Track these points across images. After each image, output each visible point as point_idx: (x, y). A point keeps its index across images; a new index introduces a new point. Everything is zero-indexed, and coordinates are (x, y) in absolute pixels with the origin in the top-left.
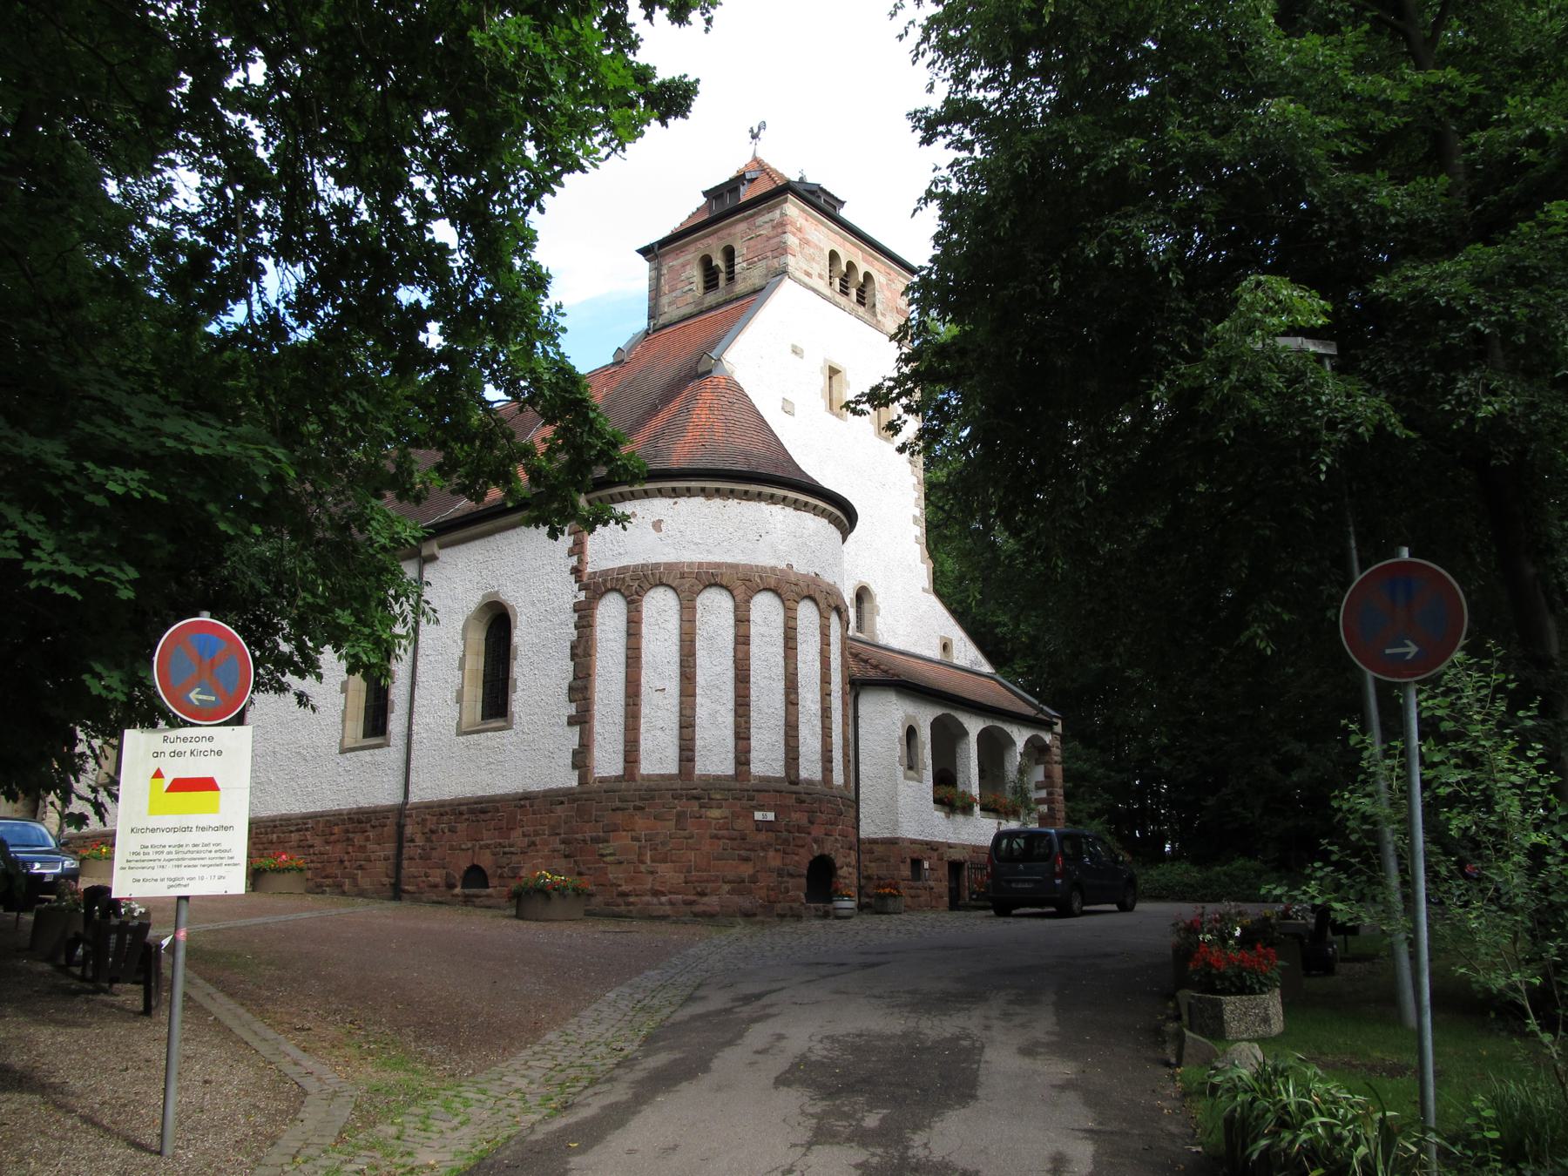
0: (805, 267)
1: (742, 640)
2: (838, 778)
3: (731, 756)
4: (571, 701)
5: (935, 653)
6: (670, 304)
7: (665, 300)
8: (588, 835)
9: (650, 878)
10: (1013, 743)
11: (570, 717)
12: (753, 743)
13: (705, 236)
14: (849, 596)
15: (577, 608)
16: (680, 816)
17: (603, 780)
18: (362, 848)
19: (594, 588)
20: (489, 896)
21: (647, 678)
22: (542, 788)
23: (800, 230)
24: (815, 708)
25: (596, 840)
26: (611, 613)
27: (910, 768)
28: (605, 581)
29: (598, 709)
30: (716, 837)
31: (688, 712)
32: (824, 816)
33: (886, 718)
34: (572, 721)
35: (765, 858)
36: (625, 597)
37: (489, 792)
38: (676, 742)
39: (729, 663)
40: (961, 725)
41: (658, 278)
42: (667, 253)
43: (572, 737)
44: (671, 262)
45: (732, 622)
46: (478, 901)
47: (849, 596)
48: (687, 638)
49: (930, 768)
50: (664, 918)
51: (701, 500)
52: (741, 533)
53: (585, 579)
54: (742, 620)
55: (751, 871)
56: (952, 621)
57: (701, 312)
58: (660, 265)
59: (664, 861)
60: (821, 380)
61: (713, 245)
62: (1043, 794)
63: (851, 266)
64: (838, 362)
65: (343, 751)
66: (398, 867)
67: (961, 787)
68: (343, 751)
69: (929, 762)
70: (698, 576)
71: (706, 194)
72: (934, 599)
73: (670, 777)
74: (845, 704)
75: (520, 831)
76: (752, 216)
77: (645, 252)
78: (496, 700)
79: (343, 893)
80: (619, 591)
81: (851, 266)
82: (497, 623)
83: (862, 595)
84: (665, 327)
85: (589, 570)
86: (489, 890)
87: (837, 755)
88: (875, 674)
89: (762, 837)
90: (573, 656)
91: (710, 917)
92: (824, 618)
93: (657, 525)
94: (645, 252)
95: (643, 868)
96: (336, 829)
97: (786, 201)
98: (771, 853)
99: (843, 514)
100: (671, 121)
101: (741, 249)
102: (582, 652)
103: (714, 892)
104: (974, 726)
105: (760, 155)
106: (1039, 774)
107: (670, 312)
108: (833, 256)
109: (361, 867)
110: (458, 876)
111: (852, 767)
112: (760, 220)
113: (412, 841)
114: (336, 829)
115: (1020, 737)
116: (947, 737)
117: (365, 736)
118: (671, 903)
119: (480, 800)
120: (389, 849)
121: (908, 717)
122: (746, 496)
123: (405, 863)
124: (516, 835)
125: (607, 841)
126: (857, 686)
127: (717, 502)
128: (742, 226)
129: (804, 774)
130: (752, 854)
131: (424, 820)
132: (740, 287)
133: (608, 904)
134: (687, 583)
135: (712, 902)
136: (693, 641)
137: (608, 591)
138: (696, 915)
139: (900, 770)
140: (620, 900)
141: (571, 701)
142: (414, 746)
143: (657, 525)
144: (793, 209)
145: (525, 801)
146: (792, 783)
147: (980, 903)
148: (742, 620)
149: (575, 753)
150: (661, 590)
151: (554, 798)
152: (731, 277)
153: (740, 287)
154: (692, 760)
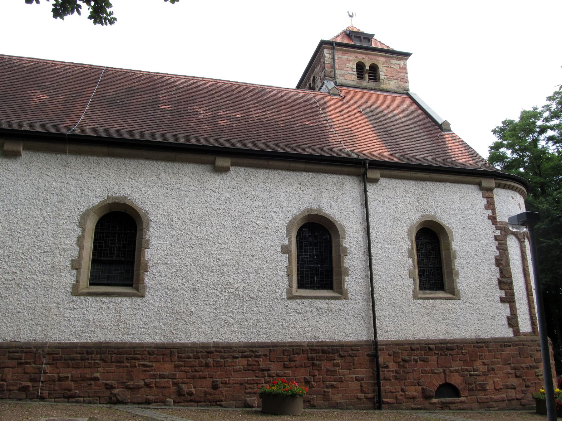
13: (361, 53)
20: (461, 402)
37: (448, 337)
43: (506, 310)
46: (452, 406)
66: (378, 384)
79: (313, 407)
86: (463, 399)
96: (297, 357)
100: (65, 17)
109: (332, 386)
119: (443, 342)
124: (478, 364)
142: (377, 303)
145: (480, 345)
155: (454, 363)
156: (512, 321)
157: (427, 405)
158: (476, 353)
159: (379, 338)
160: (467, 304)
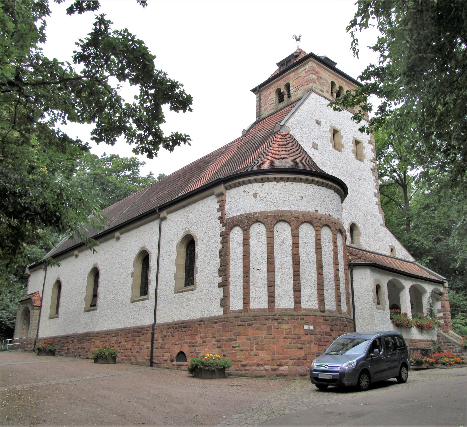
0: (320, 88)
1: (296, 245)
2: (344, 308)
3: (292, 299)
4: (220, 276)
5: (388, 253)
6: (264, 110)
7: (263, 109)
8: (228, 338)
9: (256, 357)
10: (425, 291)
11: (219, 284)
12: (302, 293)
14: (346, 227)
15: (222, 234)
16: (269, 328)
17: (234, 312)
18: (139, 343)
19: (228, 225)
21: (253, 265)
22: (208, 316)
23: (317, 73)
24: (332, 276)
25: (231, 340)
26: (236, 235)
27: (379, 304)
28: (233, 222)
29: (232, 279)
30: (286, 338)
31: (271, 279)
32: (338, 327)
33: (365, 280)
34: (220, 285)
35: (310, 348)
38: (267, 293)
39: (290, 256)
40: (401, 284)
41: (260, 100)
42: (262, 91)
43: (220, 293)
44: (265, 93)
45: (291, 237)
47: (346, 227)
48: (270, 245)
49: (388, 304)
50: (262, 377)
51: (275, 183)
52: (293, 197)
53: (225, 222)
54: (295, 236)
55: (303, 354)
56: (394, 239)
57: (277, 111)
58: (260, 95)
59: (262, 349)
60: (330, 135)
61: (281, 84)
62: (441, 315)
63: (340, 88)
64: (337, 127)
65: (132, 302)
67: (338, 378)
68: (132, 302)
69: (387, 300)
70: (274, 217)
71: (278, 64)
72: (385, 229)
73: (264, 310)
74: (346, 275)
75: (199, 336)
76: (297, 69)
77: (254, 91)
78: (189, 276)
79: (132, 363)
80: (238, 226)
81: (340, 88)
82: (189, 243)
83: (353, 227)
84: (263, 119)
85: (226, 217)
87: (343, 298)
88: (359, 261)
89: (308, 337)
90: (220, 256)
91: (284, 376)
92: (334, 235)
93: (255, 195)
94: (254, 91)
95: (252, 353)
98: (313, 345)
99: (341, 189)
101: (292, 84)
102: (224, 254)
103: (286, 364)
104: (407, 284)
105: (300, 47)
106: (438, 305)
107: (265, 113)
108: (333, 84)
110: (175, 356)
111: (351, 304)
112: (300, 71)
113: (157, 340)
115: (429, 288)
116: (395, 290)
117: (141, 295)
118: (266, 370)
119: (183, 322)
120: (149, 344)
121: (376, 280)
122: (295, 180)
123: (154, 350)
124: (198, 337)
125: (235, 340)
126: (351, 266)
127: (281, 184)
128: (293, 74)
129: (327, 307)
130: (304, 346)
131: (162, 331)
132: (293, 99)
133: (236, 370)
134: (269, 220)
135: (284, 368)
136: (273, 247)
138: (277, 376)
139: (374, 305)
140: (242, 368)
141: (220, 276)
143: (255, 195)
146: (322, 312)
147: (416, 367)
148: (295, 236)
149: (222, 300)
150: (257, 224)
151: (214, 320)
152: (289, 96)
153: (293, 99)
154: (274, 302)
155: (186, 337)
156: (224, 302)
157: (171, 366)
158: (197, 329)
159: (158, 322)
160: (199, 292)
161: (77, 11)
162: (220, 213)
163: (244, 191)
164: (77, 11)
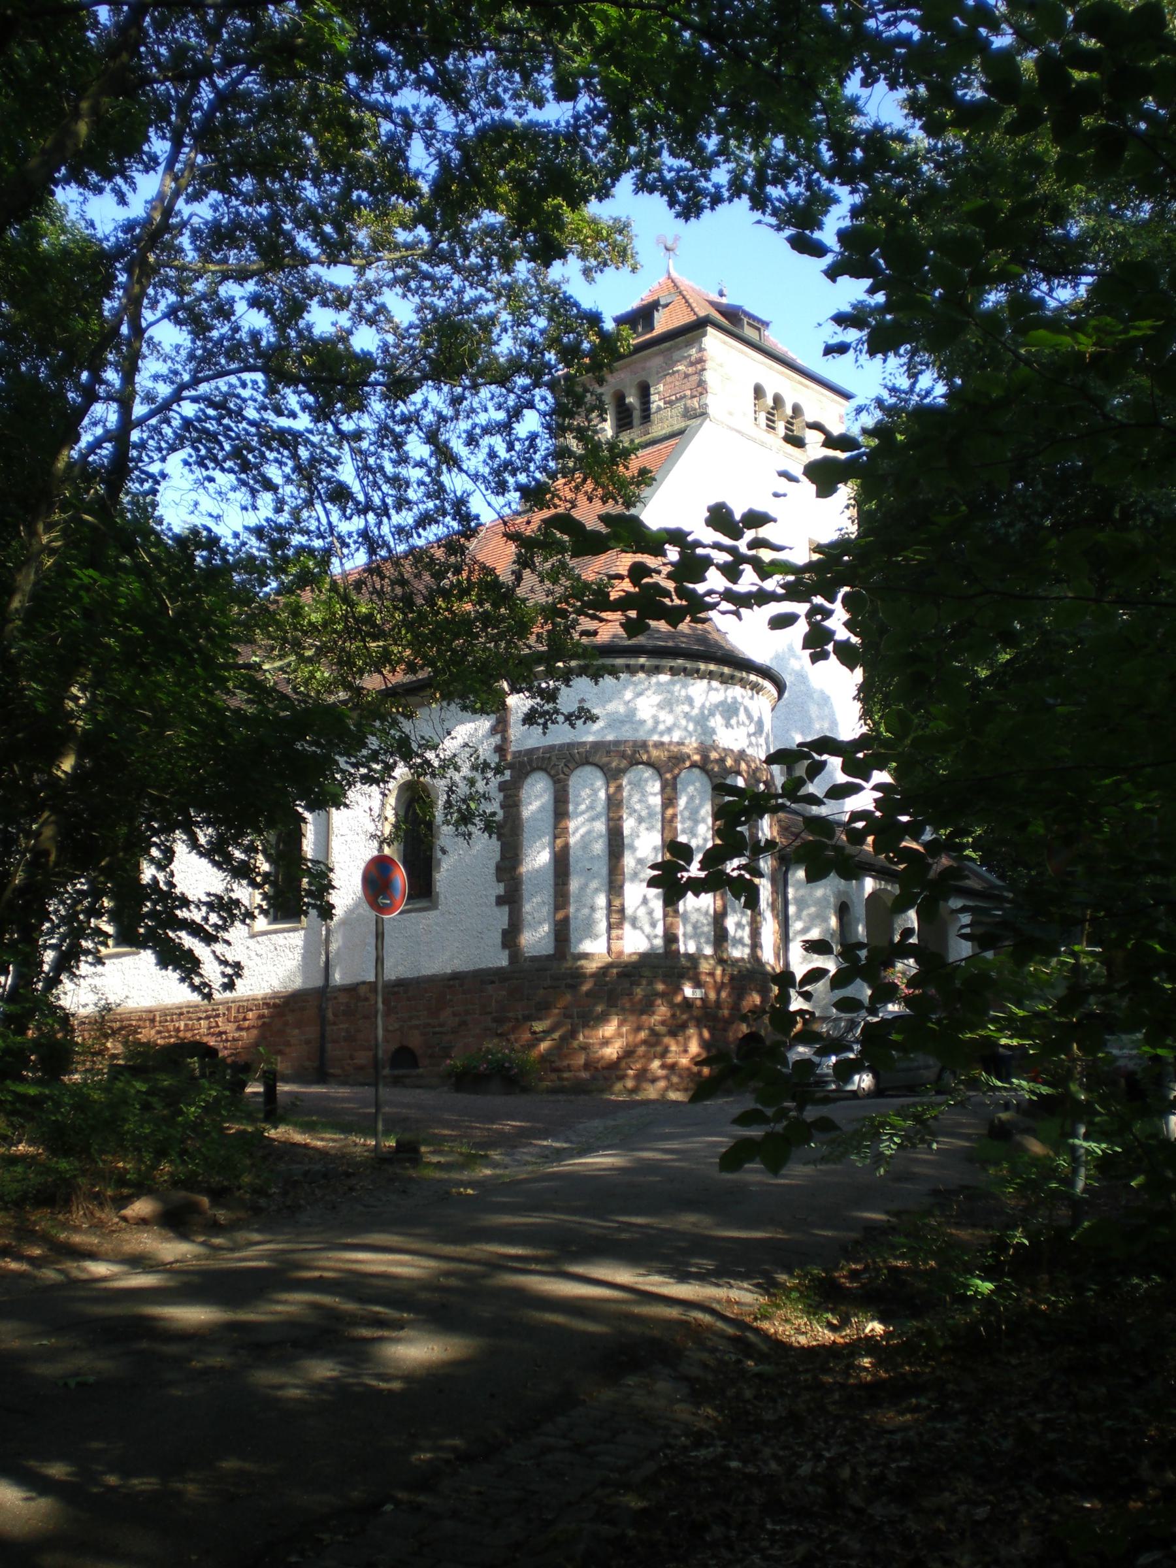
4: (499, 881)
22: (472, 968)
28: (530, 761)
34: (500, 901)
36: (552, 777)
43: (502, 917)
76: (669, 349)
80: (545, 770)
86: (421, 1070)
96: (250, 1015)
97: (704, 334)
114: (250, 1015)
121: (839, 894)
123: (329, 1046)
132: (658, 429)
137: (533, 770)
141: (499, 881)
144: (714, 342)
149: (505, 933)
152: (646, 417)
156: (510, 936)
161: (856, 121)
162: (498, 737)
163: (721, 295)
164: (856, 121)
